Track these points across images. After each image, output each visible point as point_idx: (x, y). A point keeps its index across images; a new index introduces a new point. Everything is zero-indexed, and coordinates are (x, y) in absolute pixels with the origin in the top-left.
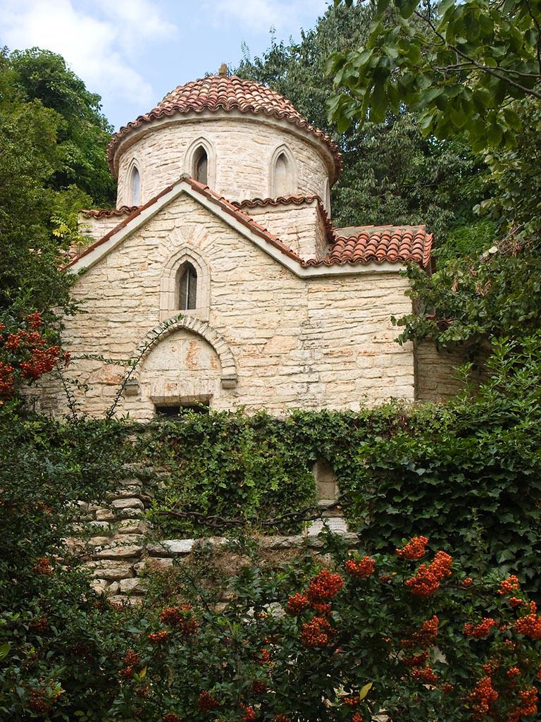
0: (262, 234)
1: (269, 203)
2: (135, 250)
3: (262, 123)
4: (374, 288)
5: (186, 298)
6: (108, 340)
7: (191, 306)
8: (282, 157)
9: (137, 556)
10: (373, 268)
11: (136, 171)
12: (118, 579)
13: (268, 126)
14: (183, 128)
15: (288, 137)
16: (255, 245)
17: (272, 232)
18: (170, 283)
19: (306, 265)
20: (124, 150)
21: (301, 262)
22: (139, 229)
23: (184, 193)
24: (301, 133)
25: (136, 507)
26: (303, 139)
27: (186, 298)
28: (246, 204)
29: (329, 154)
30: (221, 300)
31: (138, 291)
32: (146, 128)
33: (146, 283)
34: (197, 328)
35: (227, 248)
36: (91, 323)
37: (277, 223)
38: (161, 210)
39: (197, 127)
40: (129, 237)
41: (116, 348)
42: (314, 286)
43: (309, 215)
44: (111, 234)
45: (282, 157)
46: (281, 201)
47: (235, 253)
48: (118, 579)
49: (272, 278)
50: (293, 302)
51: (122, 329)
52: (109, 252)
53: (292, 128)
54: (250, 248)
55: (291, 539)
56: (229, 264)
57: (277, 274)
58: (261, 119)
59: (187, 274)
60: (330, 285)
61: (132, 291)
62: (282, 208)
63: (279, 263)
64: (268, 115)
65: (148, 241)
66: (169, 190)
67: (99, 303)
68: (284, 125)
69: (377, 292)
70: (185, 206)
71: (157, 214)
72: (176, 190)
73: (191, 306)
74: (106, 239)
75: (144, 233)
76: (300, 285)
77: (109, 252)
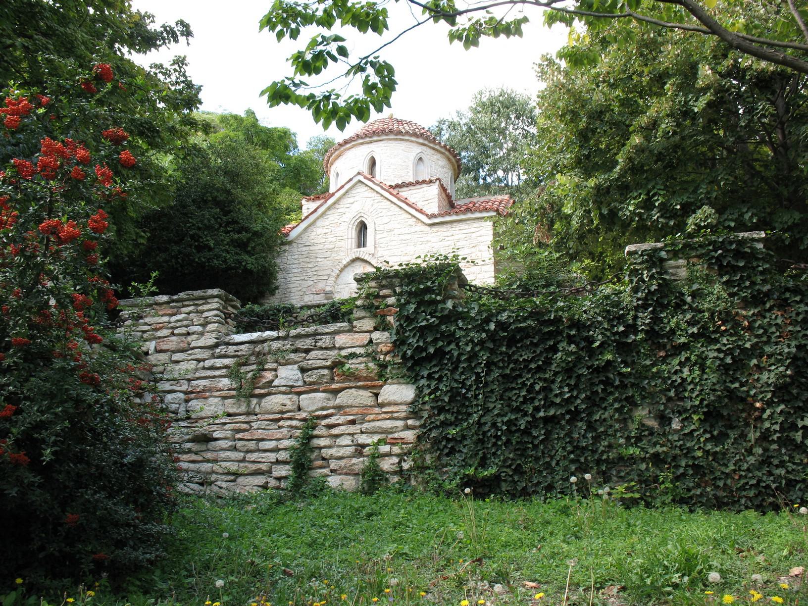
0: (405, 201)
1: (410, 184)
2: (332, 217)
3: (408, 140)
4: (472, 227)
5: (361, 241)
6: (316, 269)
7: (364, 246)
8: (421, 159)
9: (216, 345)
10: (470, 215)
11: (338, 174)
12: (204, 360)
13: (412, 141)
14: (362, 146)
15: (424, 148)
16: (401, 208)
17: (411, 200)
18: (353, 234)
19: (433, 216)
20: (332, 164)
21: (427, 215)
22: (334, 203)
23: (360, 181)
24: (432, 145)
25: (216, 316)
26: (434, 149)
27: (361, 241)
28: (397, 186)
29: (451, 157)
30: (382, 241)
31: (334, 239)
32: (342, 149)
33: (338, 234)
34: (366, 258)
35: (384, 211)
36: (308, 260)
37: (412, 195)
38: (347, 192)
39: (370, 145)
40: (329, 208)
41: (320, 273)
42: (435, 229)
43: (434, 190)
44: (318, 208)
45: (421, 159)
46: (418, 183)
47: (390, 213)
48: (204, 360)
49: (411, 226)
50: (422, 239)
51: (325, 261)
52: (318, 218)
53: (426, 142)
54: (398, 209)
55: (307, 329)
56: (386, 220)
57: (413, 224)
58: (407, 138)
59: (362, 228)
60: (444, 228)
61: (330, 240)
62: (418, 186)
63: (415, 217)
64: (411, 135)
65: (339, 211)
66: (351, 180)
67: (311, 248)
68: (421, 141)
69: (473, 230)
70: (361, 189)
71: (344, 194)
72: (355, 180)
73: (364, 246)
74: (315, 211)
75: (337, 206)
76: (428, 228)
77: (318, 218)
